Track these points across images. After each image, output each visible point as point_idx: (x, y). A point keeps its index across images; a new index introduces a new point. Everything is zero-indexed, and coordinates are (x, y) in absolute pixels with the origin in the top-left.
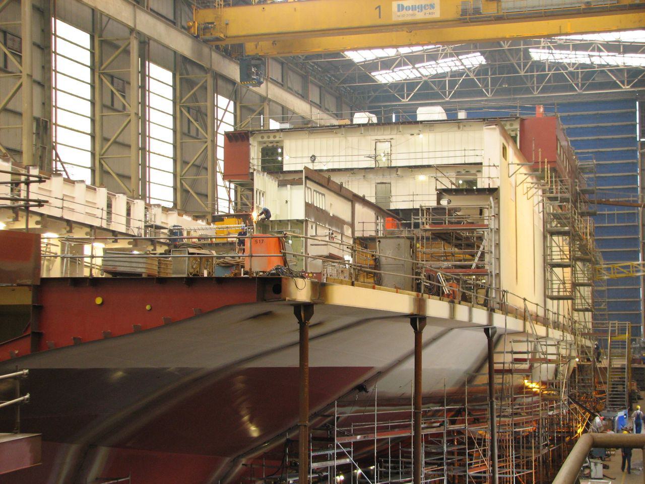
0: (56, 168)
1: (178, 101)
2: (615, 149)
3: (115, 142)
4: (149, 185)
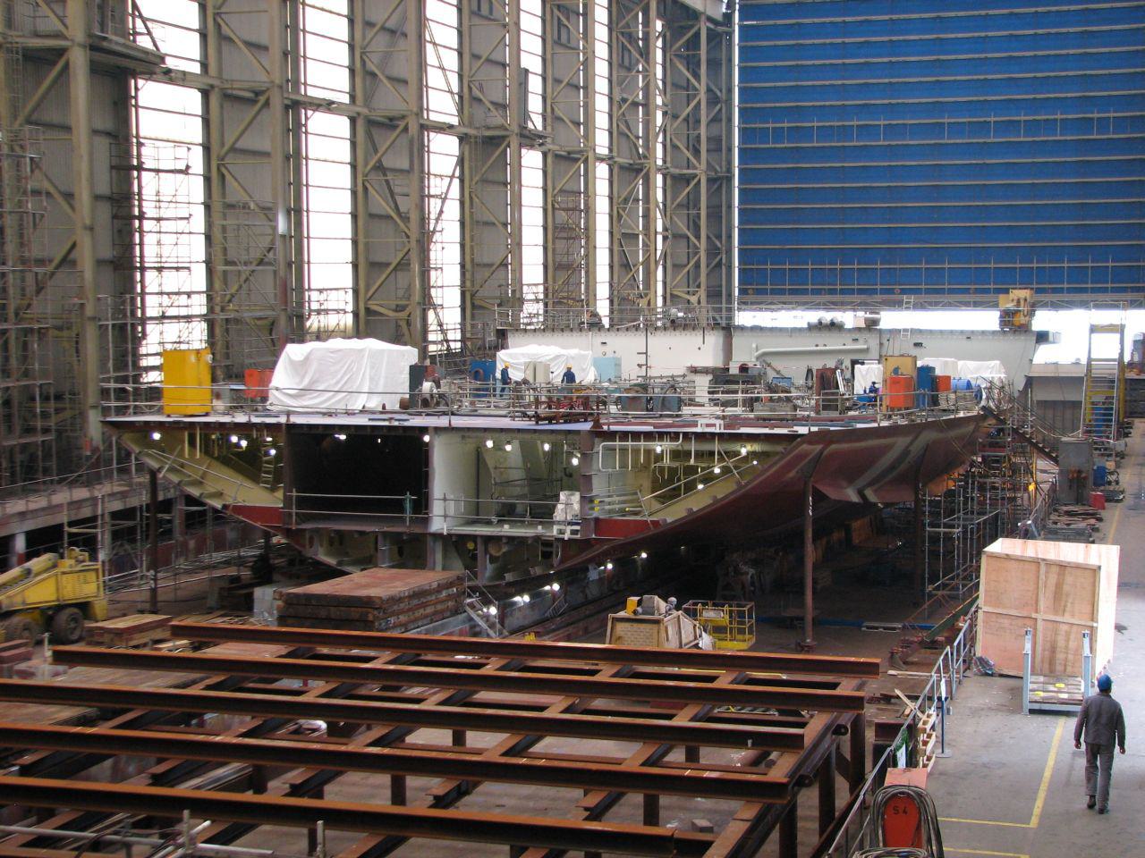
0: (134, 28)
1: (614, 25)
2: (1114, 5)
4: (305, 62)
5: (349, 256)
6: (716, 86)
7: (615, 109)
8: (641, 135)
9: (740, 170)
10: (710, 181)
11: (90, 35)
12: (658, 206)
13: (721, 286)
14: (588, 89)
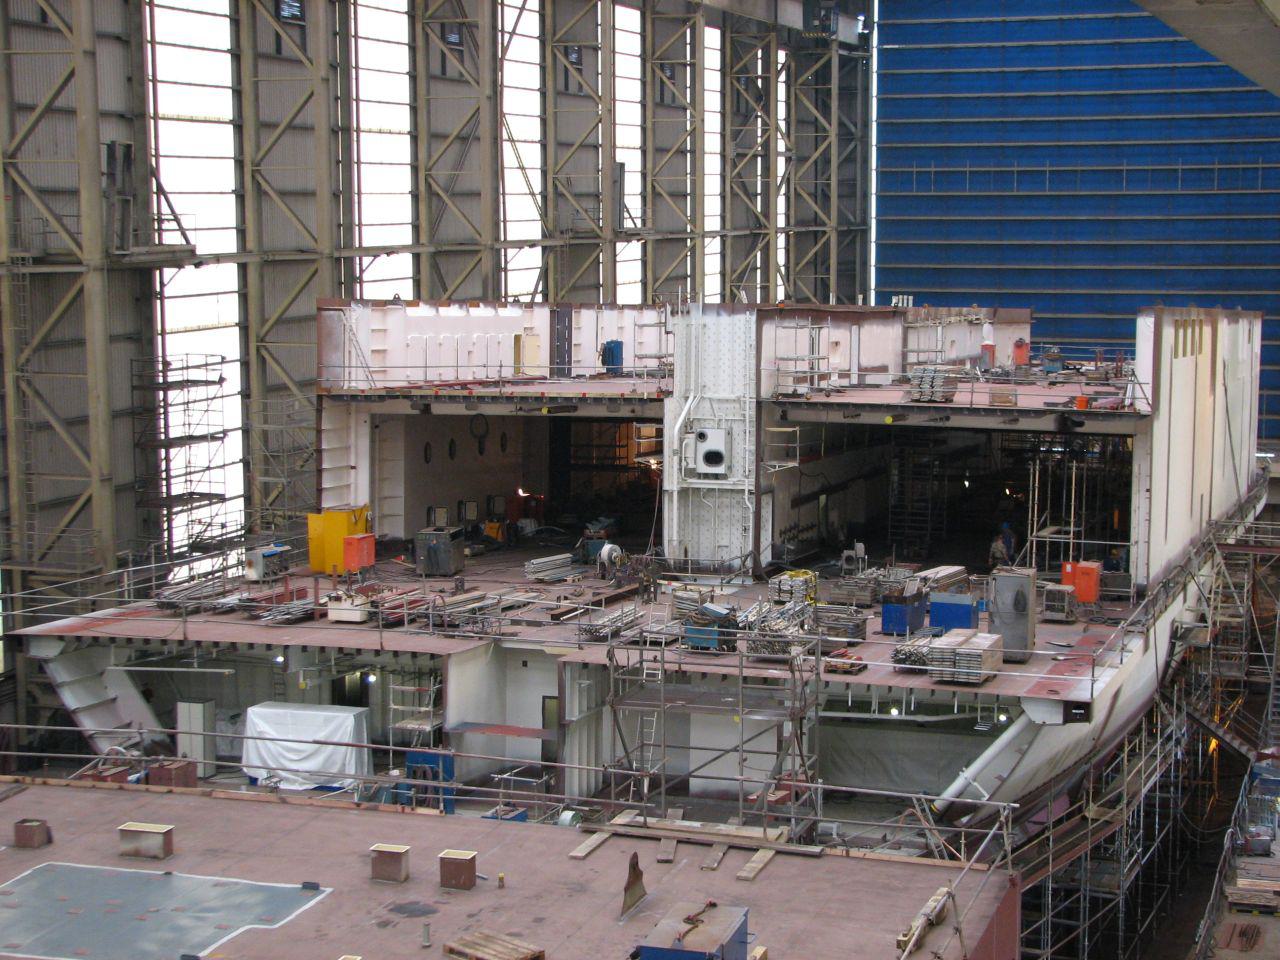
3: (291, 127)
5: (407, 186)
6: (850, 120)
7: (728, 168)
8: (759, 191)
9: (879, 222)
10: (841, 235)
11: (107, 254)
12: (779, 271)
13: (854, 263)
14: (697, 153)
